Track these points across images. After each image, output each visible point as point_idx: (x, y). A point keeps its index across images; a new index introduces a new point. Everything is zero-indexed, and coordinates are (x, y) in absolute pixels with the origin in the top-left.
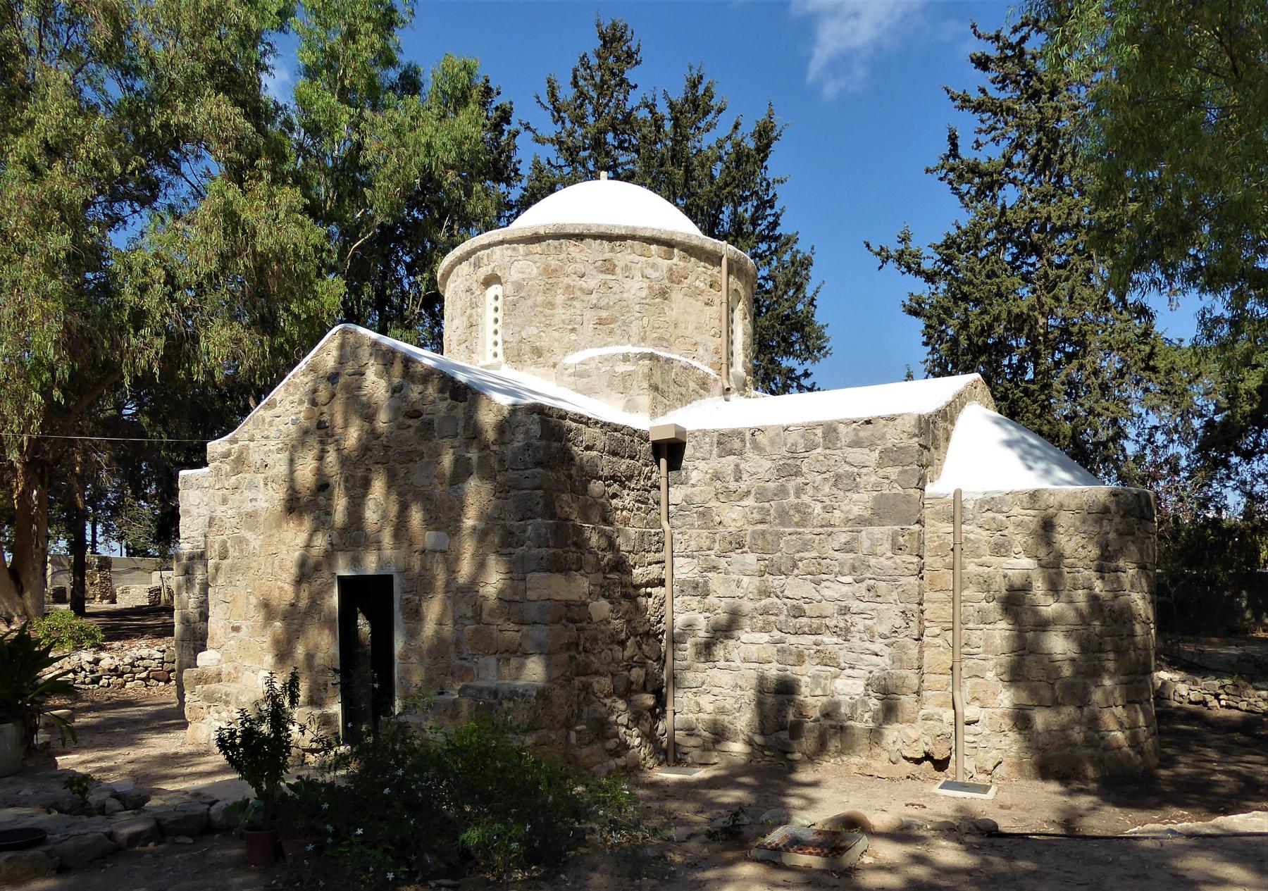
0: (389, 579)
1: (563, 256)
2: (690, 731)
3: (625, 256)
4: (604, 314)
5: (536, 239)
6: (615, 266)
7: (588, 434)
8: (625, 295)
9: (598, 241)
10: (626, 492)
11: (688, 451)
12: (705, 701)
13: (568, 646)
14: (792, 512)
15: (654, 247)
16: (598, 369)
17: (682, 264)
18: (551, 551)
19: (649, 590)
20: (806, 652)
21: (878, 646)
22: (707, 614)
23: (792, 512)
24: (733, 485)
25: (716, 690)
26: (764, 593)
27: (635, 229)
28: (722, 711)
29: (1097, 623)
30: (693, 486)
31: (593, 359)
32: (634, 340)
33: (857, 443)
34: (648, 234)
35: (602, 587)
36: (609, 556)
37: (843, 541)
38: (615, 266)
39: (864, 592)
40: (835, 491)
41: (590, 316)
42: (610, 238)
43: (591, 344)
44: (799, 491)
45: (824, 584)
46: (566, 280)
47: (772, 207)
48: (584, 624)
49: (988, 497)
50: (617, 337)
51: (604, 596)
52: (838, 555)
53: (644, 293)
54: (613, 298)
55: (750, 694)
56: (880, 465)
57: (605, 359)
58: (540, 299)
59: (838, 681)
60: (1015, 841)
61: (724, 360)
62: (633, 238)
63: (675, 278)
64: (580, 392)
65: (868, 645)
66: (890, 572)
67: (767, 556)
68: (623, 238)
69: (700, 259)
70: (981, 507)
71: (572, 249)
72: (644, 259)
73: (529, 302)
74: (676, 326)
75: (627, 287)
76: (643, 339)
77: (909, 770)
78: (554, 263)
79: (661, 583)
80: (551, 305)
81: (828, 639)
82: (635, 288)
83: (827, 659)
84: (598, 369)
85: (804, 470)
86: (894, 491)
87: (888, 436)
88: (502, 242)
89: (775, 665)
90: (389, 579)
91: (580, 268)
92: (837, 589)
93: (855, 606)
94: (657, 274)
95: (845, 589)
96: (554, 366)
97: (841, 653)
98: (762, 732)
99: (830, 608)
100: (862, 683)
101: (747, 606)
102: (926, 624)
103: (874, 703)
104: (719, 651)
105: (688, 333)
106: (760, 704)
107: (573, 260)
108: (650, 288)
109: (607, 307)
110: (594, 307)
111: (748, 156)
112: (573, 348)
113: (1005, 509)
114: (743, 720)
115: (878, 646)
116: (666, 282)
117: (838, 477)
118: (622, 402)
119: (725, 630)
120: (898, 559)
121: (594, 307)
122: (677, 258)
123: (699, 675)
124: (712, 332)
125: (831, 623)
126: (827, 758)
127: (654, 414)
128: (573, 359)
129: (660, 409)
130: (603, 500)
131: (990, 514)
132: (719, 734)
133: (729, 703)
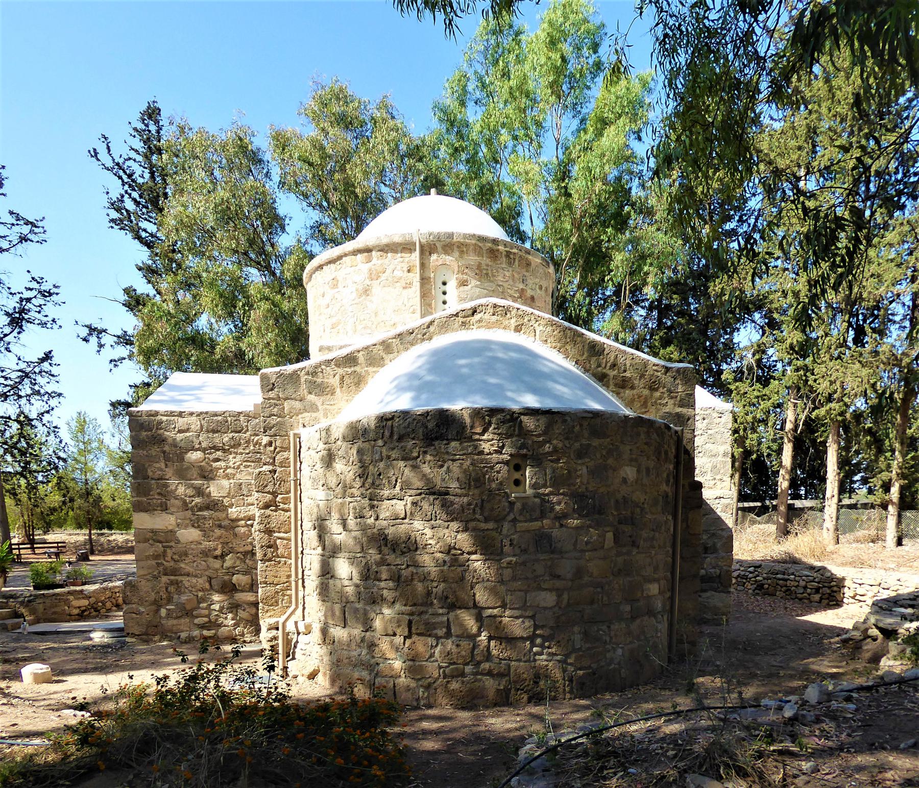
7: (181, 422)
10: (231, 457)
13: (156, 557)
17: (380, 262)
19: (249, 523)
36: (198, 500)
51: (193, 526)
53: (354, 295)
62: (346, 255)
63: (374, 276)
69: (396, 252)
116: (368, 282)
124: (411, 310)
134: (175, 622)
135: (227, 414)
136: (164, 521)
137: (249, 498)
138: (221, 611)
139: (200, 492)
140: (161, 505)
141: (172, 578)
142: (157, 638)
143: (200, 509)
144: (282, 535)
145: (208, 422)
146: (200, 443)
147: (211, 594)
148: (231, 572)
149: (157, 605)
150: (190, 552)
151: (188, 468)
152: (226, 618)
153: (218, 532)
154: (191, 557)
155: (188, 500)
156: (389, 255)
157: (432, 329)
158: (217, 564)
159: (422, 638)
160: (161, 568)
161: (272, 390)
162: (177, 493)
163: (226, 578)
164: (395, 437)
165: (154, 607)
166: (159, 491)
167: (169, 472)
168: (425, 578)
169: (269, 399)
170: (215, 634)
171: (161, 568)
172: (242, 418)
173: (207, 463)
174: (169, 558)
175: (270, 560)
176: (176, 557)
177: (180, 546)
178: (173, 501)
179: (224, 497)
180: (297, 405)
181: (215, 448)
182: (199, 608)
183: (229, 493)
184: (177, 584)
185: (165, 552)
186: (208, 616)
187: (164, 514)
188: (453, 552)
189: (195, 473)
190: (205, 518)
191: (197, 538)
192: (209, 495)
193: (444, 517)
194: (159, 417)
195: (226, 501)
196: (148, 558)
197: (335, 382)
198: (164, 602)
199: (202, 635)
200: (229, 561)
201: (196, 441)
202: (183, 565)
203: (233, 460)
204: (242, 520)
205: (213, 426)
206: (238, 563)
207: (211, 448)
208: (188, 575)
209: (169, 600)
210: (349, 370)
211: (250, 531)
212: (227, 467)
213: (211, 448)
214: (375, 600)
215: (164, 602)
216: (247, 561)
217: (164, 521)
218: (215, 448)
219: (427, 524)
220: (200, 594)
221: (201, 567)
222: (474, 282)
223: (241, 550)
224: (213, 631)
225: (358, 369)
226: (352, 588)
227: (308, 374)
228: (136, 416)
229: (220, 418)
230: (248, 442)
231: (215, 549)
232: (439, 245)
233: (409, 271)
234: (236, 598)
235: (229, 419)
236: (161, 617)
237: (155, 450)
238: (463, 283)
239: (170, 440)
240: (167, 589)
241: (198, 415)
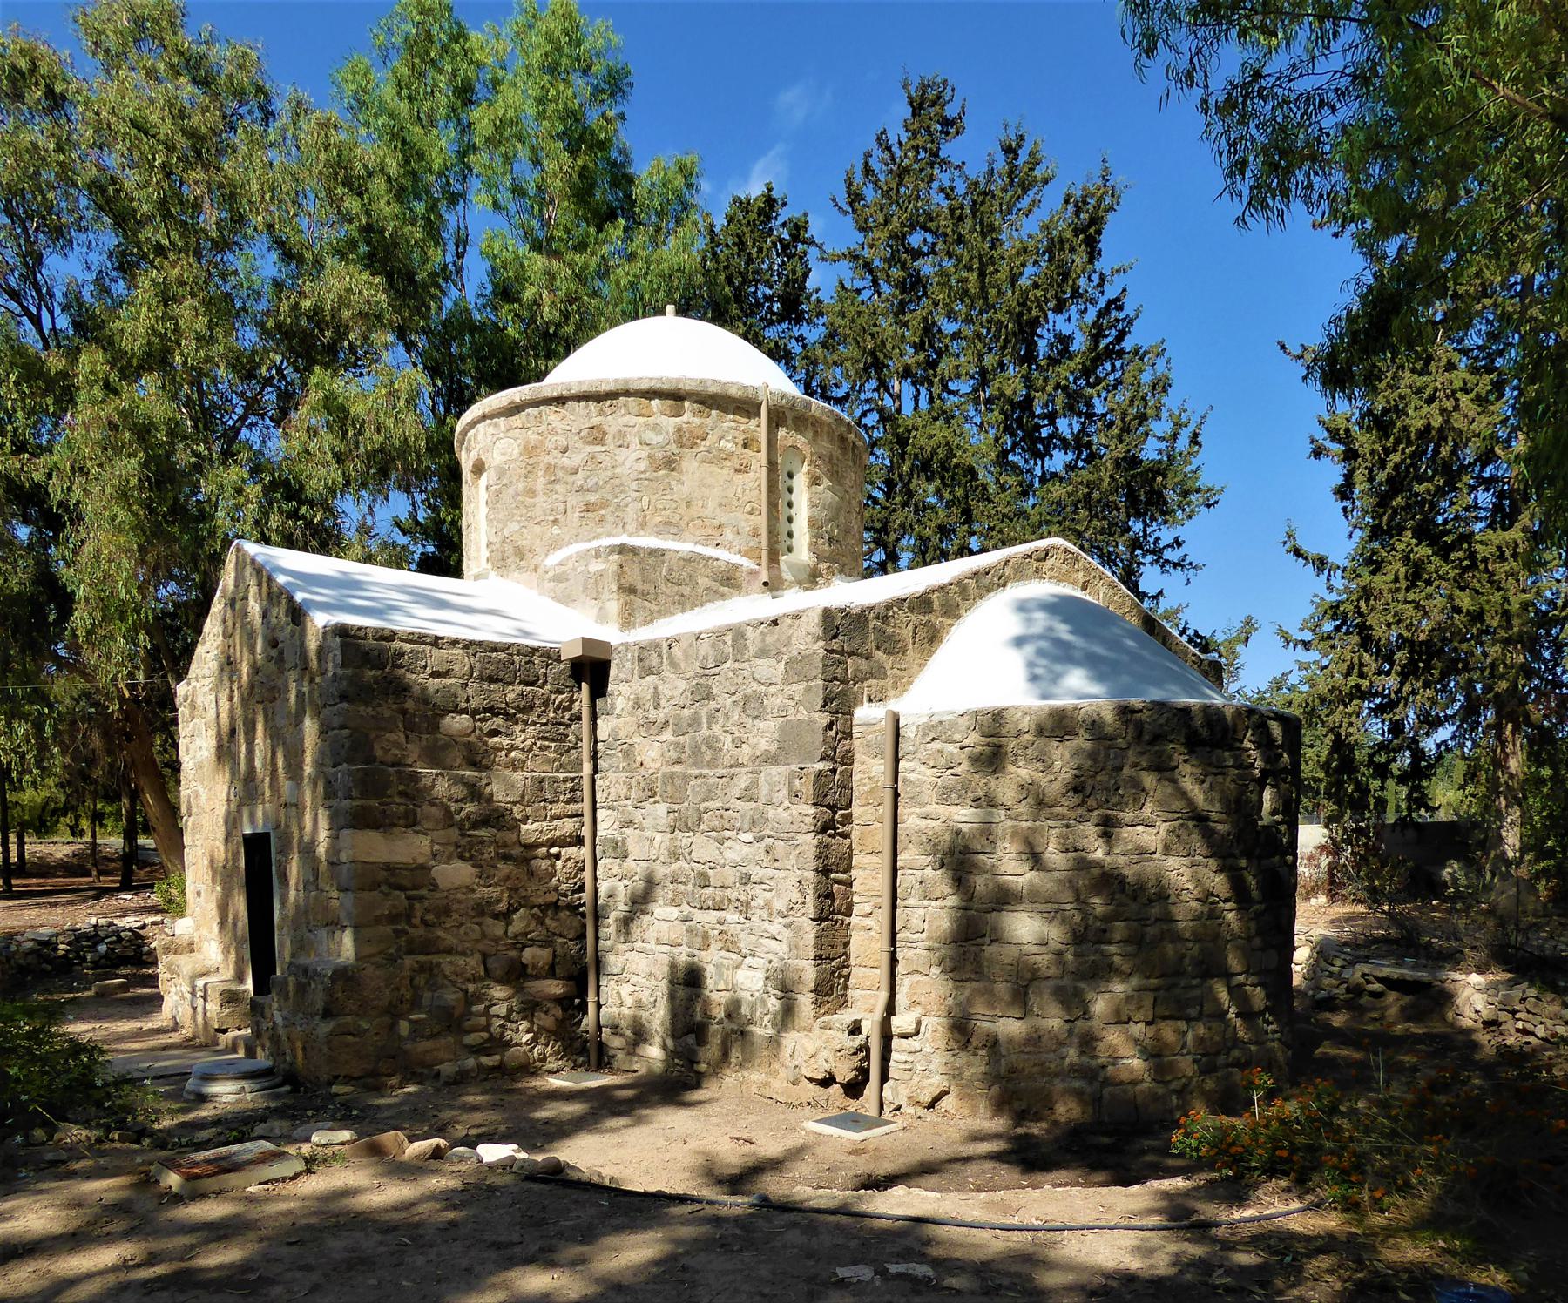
0: (267, 834)
1: (543, 427)
2: (615, 1029)
3: (618, 418)
4: (592, 498)
5: (560, 401)
6: (605, 433)
7: (436, 657)
8: (618, 470)
9: (583, 404)
10: (517, 728)
11: (613, 672)
12: (625, 990)
13: (393, 918)
14: (704, 748)
15: (655, 403)
16: (574, 569)
17: (697, 420)
18: (358, 803)
19: (554, 850)
20: (711, 933)
21: (776, 927)
22: (626, 882)
23: (704, 748)
24: (652, 714)
25: (634, 979)
26: (675, 855)
27: (627, 381)
28: (639, 1005)
29: (1096, 900)
30: (619, 716)
31: (570, 558)
32: (631, 527)
33: (763, 653)
34: (644, 386)
35: (458, 846)
36: (470, 807)
37: (743, 785)
38: (605, 433)
39: (762, 855)
40: (745, 719)
41: (576, 501)
42: (598, 397)
43: (577, 538)
44: (711, 718)
45: (727, 843)
46: (547, 459)
47: (1120, 308)
48: (424, 892)
49: (935, 719)
50: (609, 527)
51: (461, 857)
52: (740, 805)
53: (643, 465)
54: (604, 475)
55: (663, 985)
56: (786, 682)
57: (581, 556)
58: (521, 486)
59: (739, 972)
60: (636, 1200)
61: (764, 544)
62: (627, 393)
63: (686, 440)
64: (559, 601)
65: (766, 925)
66: (787, 827)
67: (676, 807)
68: (613, 395)
69: (726, 411)
70: (925, 735)
71: (553, 417)
72: (641, 420)
73: (511, 491)
74: (688, 504)
75: (620, 459)
76: (643, 526)
77: (810, 1095)
78: (534, 438)
79: (579, 841)
80: (531, 492)
81: (731, 916)
82: (631, 461)
83: (730, 945)
84: (574, 569)
85: (715, 691)
86: (799, 717)
87: (793, 641)
88: (484, 417)
89: (684, 949)
90: (267, 834)
91: (562, 441)
92: (739, 850)
93: (757, 873)
94: (660, 438)
95: (746, 849)
96: (536, 570)
97: (743, 935)
98: (674, 1036)
99: (731, 876)
100: (761, 975)
101: (661, 871)
102: (856, 898)
103: (774, 1004)
104: (636, 931)
105: (707, 512)
106: (672, 997)
107: (554, 432)
108: (650, 457)
109: (596, 488)
110: (580, 490)
111: (1061, 241)
112: (555, 545)
113: (957, 737)
114: (658, 1018)
115: (776, 927)
116: (674, 448)
117: (747, 699)
118: (596, 610)
119: (641, 902)
120: (795, 810)
121: (580, 490)
122: (690, 415)
123: (622, 959)
124: (748, 508)
125: (732, 894)
126: (728, 1072)
127: (627, 622)
128: (553, 559)
129: (639, 618)
130: (472, 739)
131: (937, 745)
132: (640, 1035)
133: (646, 997)
134: (428, 1044)
135: (514, 650)
136: (412, 847)
137: (555, 806)
138: (508, 1018)
139: (475, 792)
140: (406, 814)
141: (422, 958)
142: (394, 1081)
143: (475, 826)
144: (840, 876)
145: (482, 661)
146: (468, 700)
147: (488, 987)
148: (520, 943)
149: (393, 1013)
150: (455, 906)
151: (446, 747)
152: (517, 1030)
153: (504, 868)
154: (455, 916)
155: (453, 806)
156: (714, 412)
157: (1007, 571)
158: (497, 928)
159: (1169, 1022)
160: (403, 941)
161: (835, 637)
162: (435, 793)
163: (513, 953)
164: (1147, 737)
165: (387, 1019)
166: (401, 788)
167: (413, 752)
168: (1177, 938)
169: (832, 651)
170: (501, 1061)
171: (403, 941)
172: (537, 660)
173: (480, 739)
174: (416, 921)
175: (826, 919)
176: (430, 917)
177: (438, 895)
178: (426, 807)
179: (514, 803)
180: (864, 665)
181: (493, 711)
182: (471, 1013)
183: (522, 797)
184: (431, 969)
185: (411, 907)
186: (487, 1028)
187: (410, 834)
188: (1211, 899)
189: (456, 756)
190: (482, 842)
191: (468, 881)
192: (490, 799)
193: (1205, 851)
194: (397, 644)
195: (517, 811)
196: (378, 921)
197: (907, 632)
198: (406, 1006)
199: (480, 1066)
200: (519, 921)
201: (462, 696)
202: (441, 933)
203: (522, 735)
204: (542, 845)
205: (490, 669)
206: (533, 925)
207: (486, 710)
208: (449, 951)
209: (415, 1004)
210: (925, 619)
211: (553, 866)
212: (513, 748)
213: (486, 710)
214: (1098, 972)
215: (406, 1006)
216: (547, 921)
217: (412, 847)
218: (493, 711)
219: (1186, 861)
220: (471, 987)
221: (473, 936)
222: (826, 483)
223: (540, 901)
224: (497, 1057)
225: (931, 617)
226: (1047, 957)
227: (877, 618)
228: (355, 637)
229: (502, 656)
230: (546, 704)
231: (499, 901)
232: (789, 415)
233: (745, 446)
234: (532, 991)
235: (517, 659)
236: (400, 1037)
237: (387, 709)
238: (815, 481)
239: (416, 689)
240: (412, 980)
241: (465, 647)
